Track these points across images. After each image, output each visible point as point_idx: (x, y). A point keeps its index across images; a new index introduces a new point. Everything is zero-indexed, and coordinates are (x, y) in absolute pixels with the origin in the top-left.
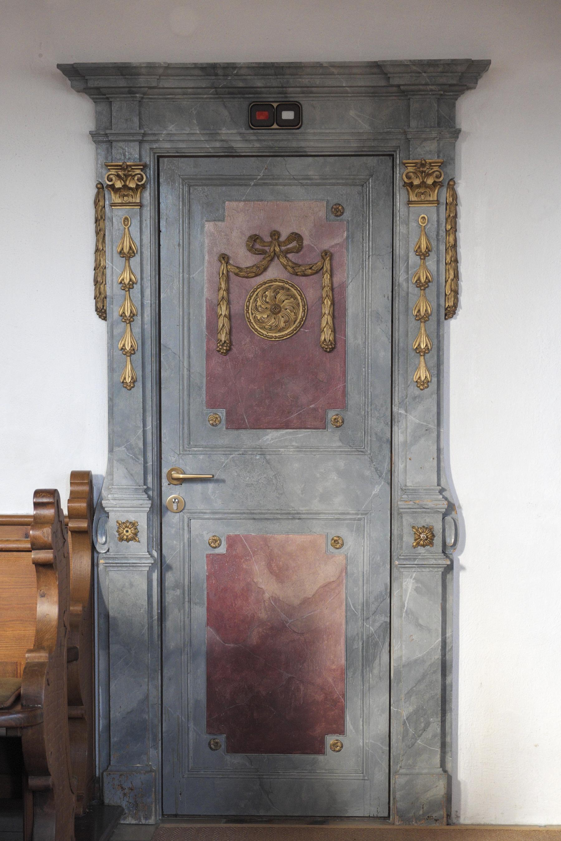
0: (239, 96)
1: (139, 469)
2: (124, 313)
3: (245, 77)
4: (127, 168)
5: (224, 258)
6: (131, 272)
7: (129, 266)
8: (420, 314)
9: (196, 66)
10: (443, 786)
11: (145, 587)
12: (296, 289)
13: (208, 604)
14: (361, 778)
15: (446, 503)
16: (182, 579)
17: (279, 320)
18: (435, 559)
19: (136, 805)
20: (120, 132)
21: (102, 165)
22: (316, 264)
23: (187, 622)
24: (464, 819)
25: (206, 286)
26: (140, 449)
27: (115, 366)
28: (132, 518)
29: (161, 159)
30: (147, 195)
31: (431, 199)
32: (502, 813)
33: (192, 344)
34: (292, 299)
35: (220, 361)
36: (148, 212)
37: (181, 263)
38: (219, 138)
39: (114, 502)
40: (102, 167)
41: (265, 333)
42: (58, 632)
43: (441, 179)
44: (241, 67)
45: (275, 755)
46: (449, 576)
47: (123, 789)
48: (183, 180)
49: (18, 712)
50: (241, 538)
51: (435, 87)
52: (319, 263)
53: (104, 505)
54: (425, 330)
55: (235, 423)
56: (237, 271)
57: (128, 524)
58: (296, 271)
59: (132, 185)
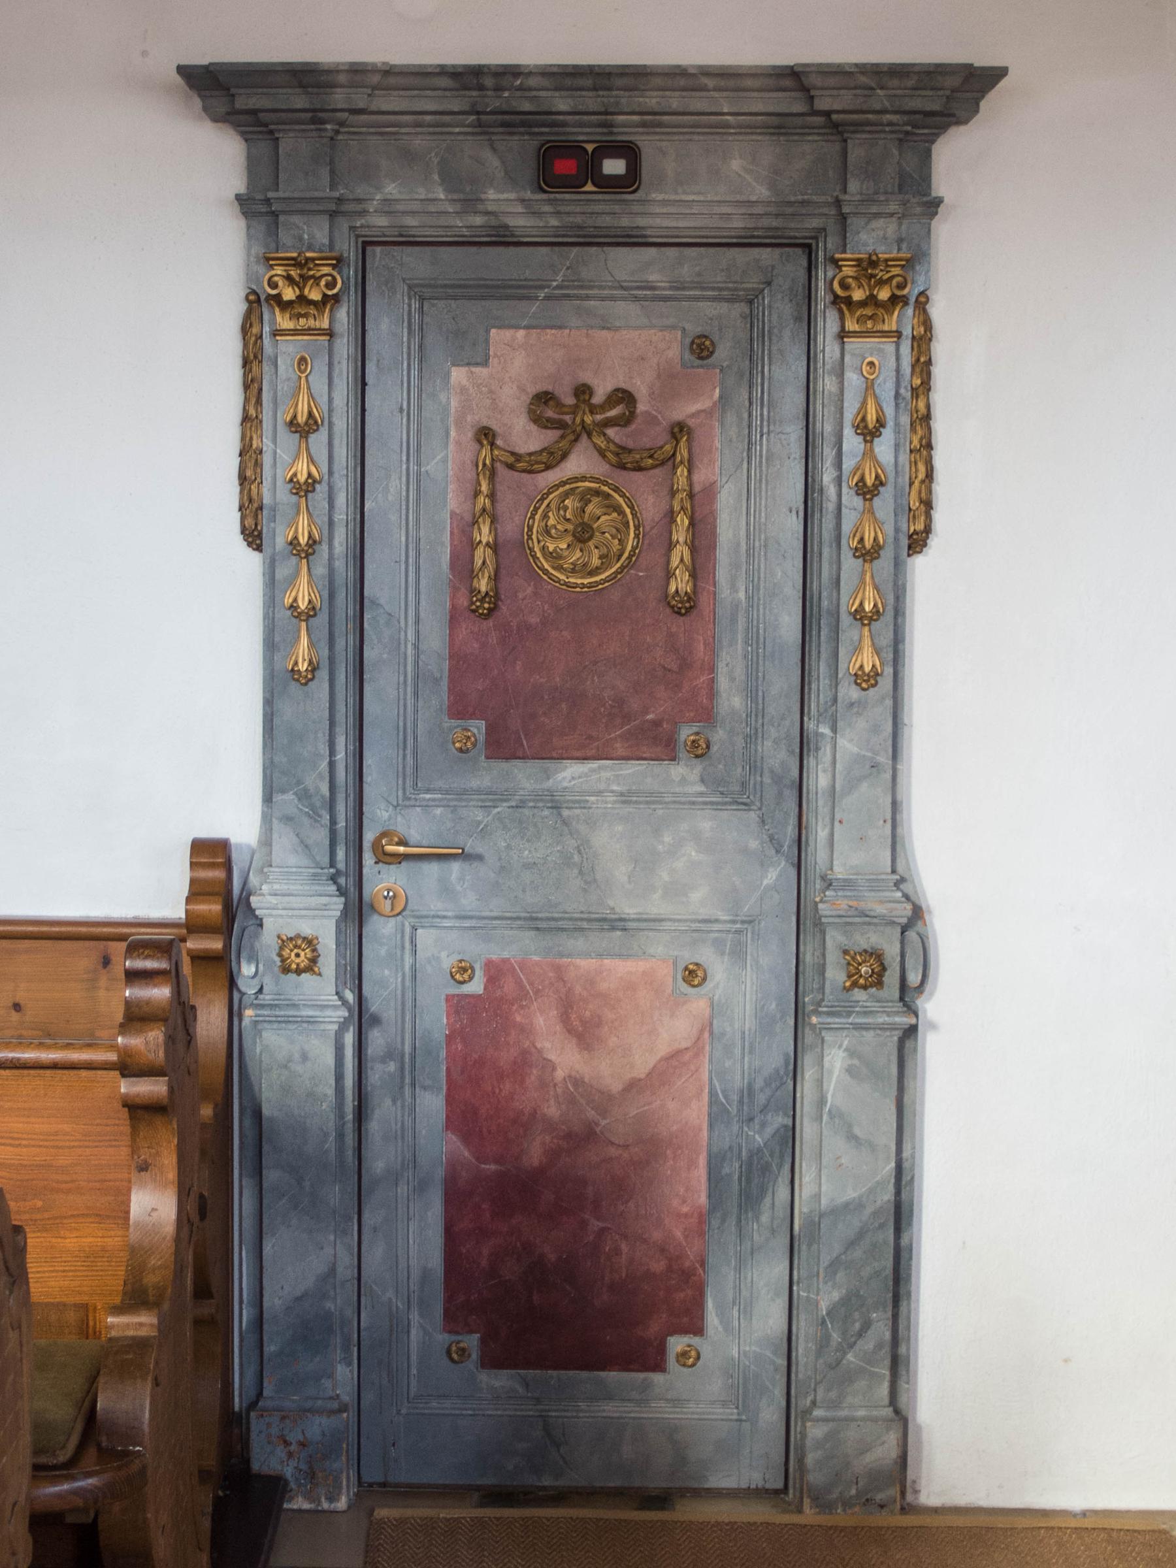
0: (522, 130)
1: (321, 836)
2: (296, 538)
3: (534, 93)
4: (306, 263)
5: (485, 435)
6: (311, 460)
7: (308, 449)
8: (864, 547)
9: (443, 71)
10: (895, 1442)
11: (330, 1059)
12: (623, 496)
13: (448, 1089)
14: (735, 1417)
15: (909, 907)
16: (399, 1039)
17: (590, 552)
18: (888, 1014)
19: (311, 1475)
20: (296, 195)
21: (257, 257)
22: (662, 447)
23: (408, 1122)
24: (928, 1496)
25: (451, 487)
26: (323, 797)
27: (277, 639)
28: (306, 929)
29: (369, 249)
30: (343, 315)
31: (886, 328)
32: (1000, 1487)
33: (423, 597)
34: (615, 515)
35: (476, 630)
36: (344, 347)
37: (405, 444)
38: (480, 207)
39: (274, 900)
40: (258, 262)
41: (562, 577)
42: (177, 1252)
43: (905, 292)
44: (530, 73)
45: (571, 1373)
46: (909, 1044)
47: (287, 1443)
48: (410, 287)
49: (88, 1475)
50: (511, 964)
51: (898, 116)
52: (668, 447)
53: (253, 905)
54: (872, 577)
55: (501, 746)
56: (511, 460)
57: (299, 942)
58: (624, 460)
59: (315, 296)
